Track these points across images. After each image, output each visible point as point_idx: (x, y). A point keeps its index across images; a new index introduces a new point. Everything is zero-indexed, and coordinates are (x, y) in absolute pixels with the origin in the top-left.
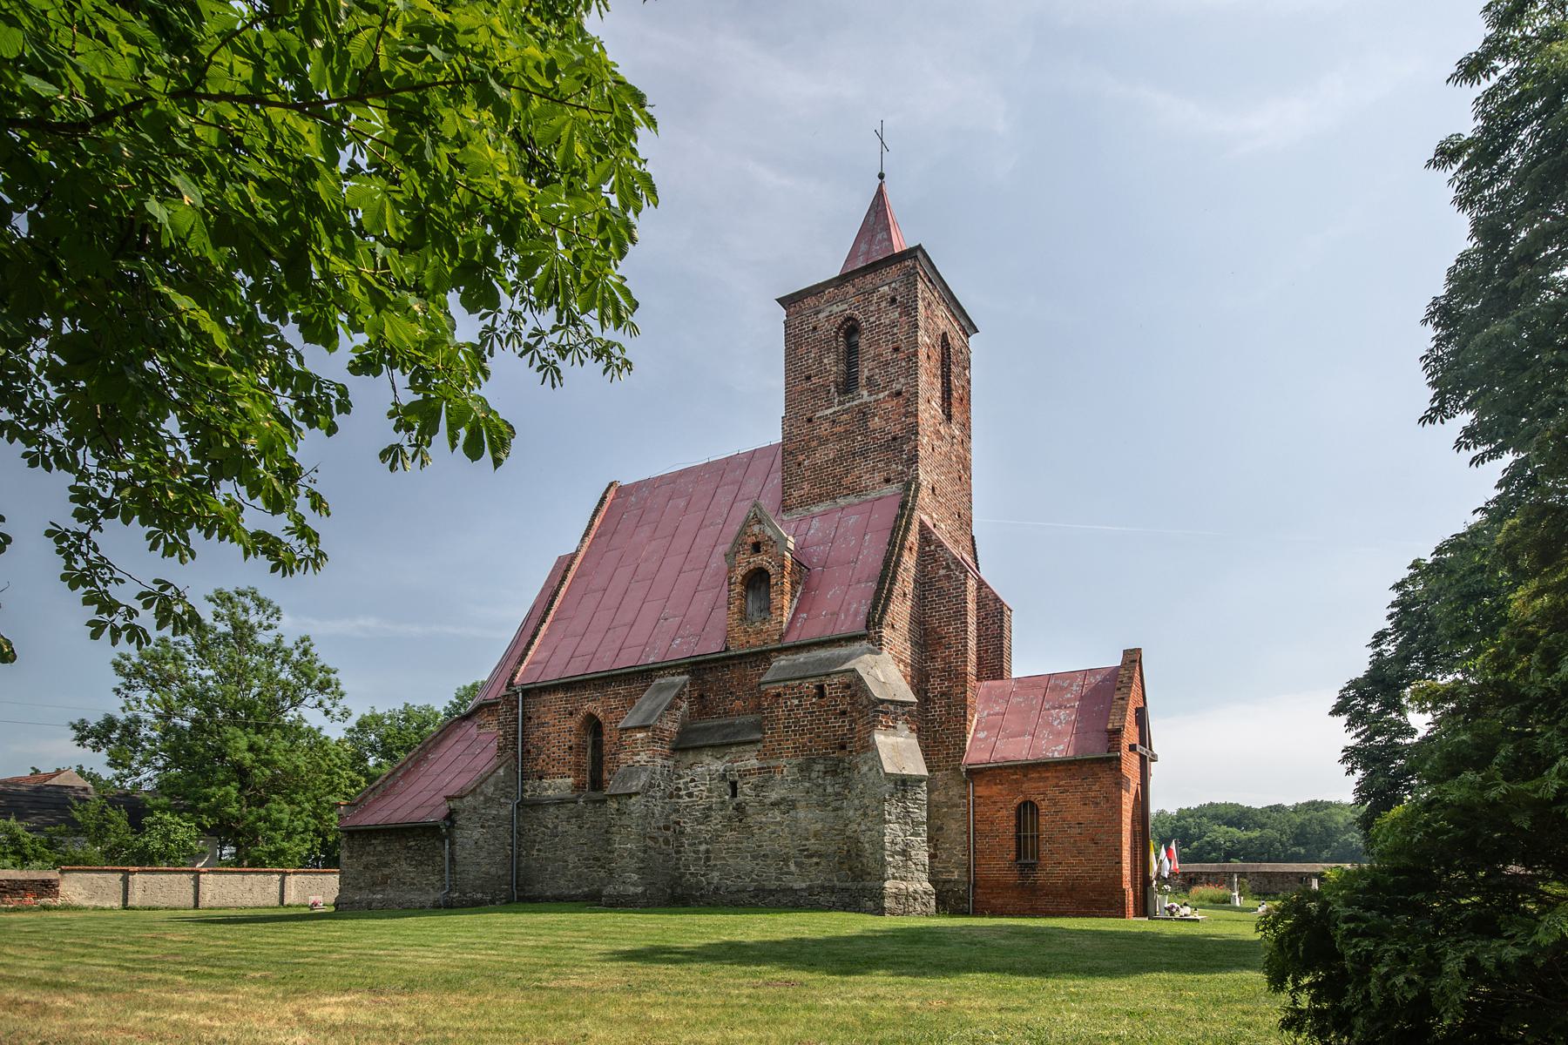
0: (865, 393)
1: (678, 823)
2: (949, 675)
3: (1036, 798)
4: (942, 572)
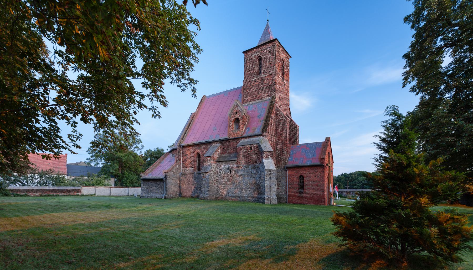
0: (263, 75)
4: (281, 118)
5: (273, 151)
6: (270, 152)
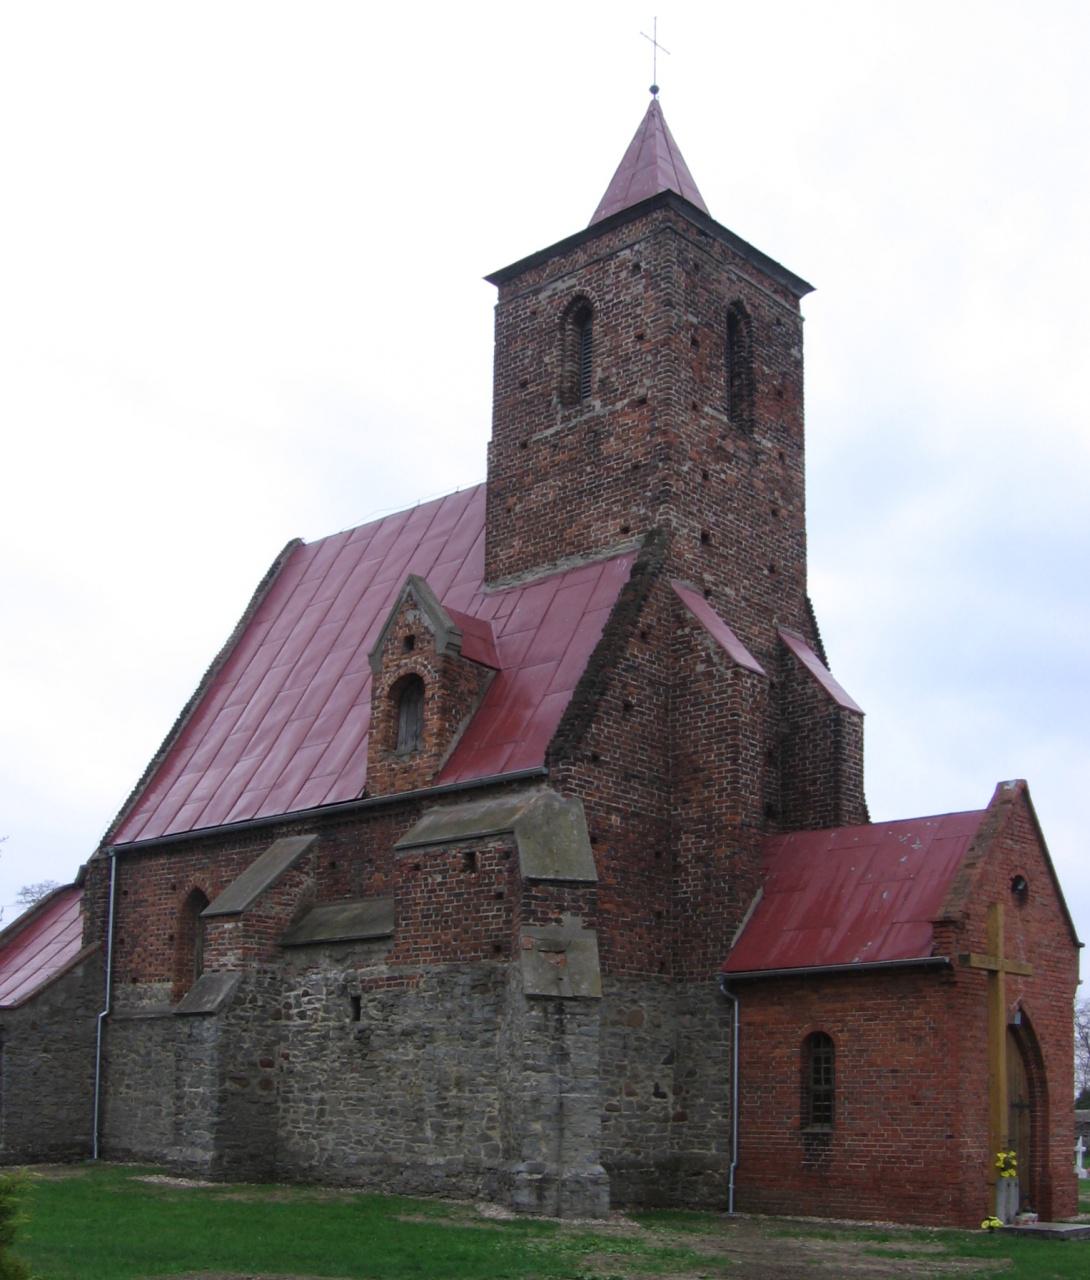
0: (597, 403)
1: (286, 1057)
2: (709, 829)
3: (828, 1027)
4: (701, 668)
5: (594, 877)
6: (573, 884)
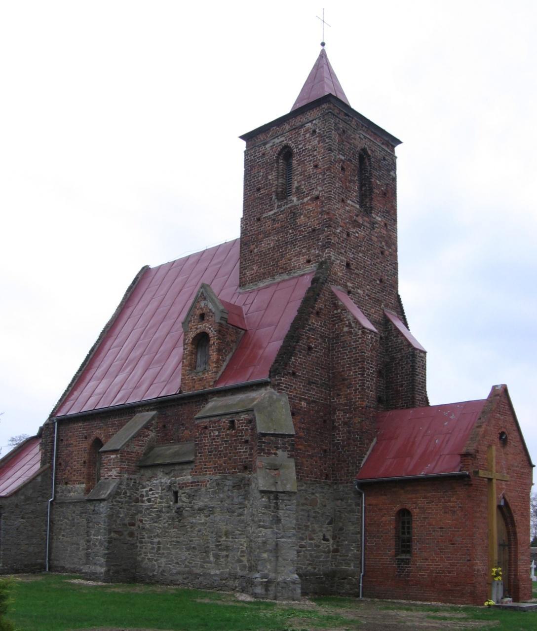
0: (295, 199)
1: (141, 521)
2: (350, 409)
3: (409, 506)
4: (346, 329)
5: (293, 432)
6: (283, 436)
